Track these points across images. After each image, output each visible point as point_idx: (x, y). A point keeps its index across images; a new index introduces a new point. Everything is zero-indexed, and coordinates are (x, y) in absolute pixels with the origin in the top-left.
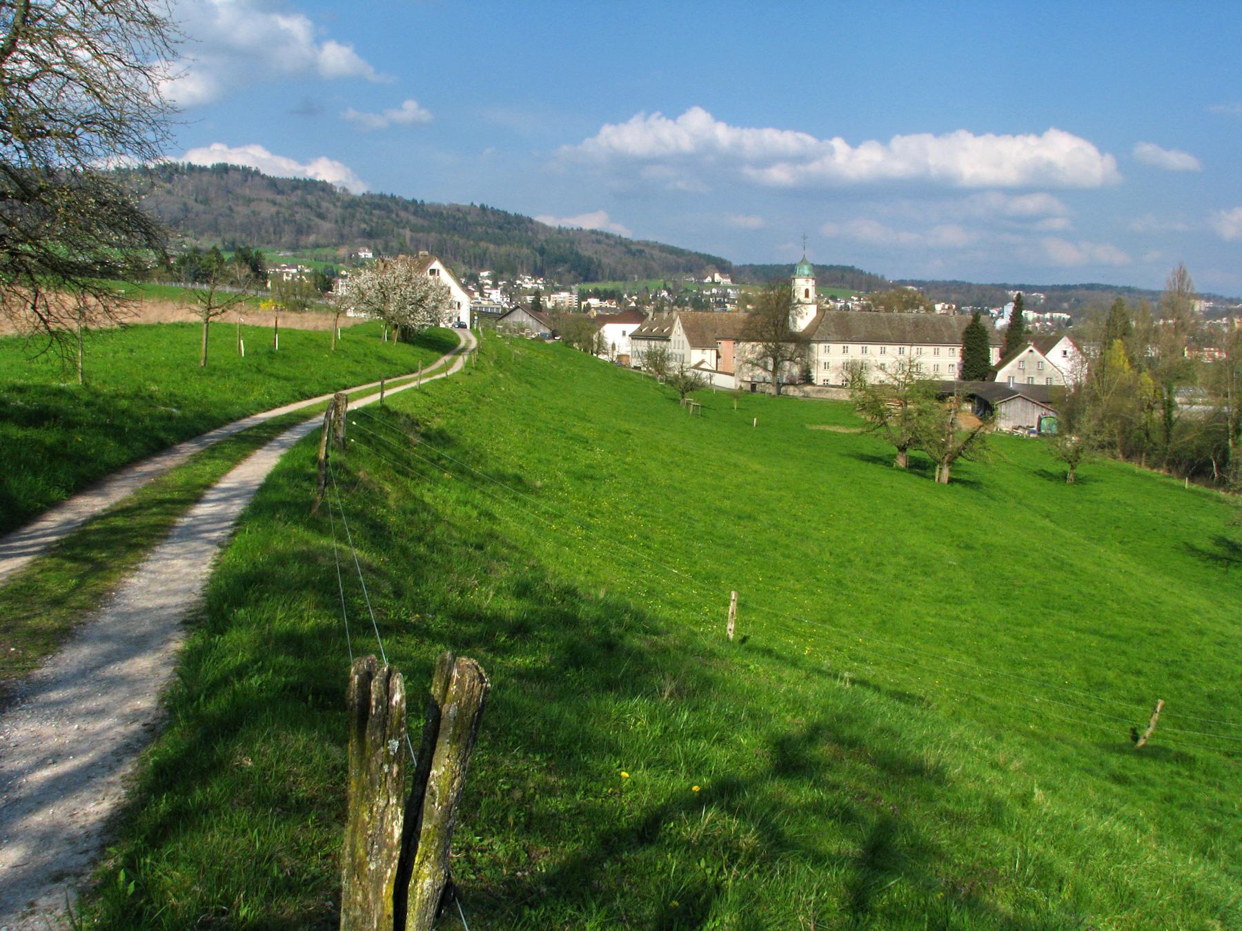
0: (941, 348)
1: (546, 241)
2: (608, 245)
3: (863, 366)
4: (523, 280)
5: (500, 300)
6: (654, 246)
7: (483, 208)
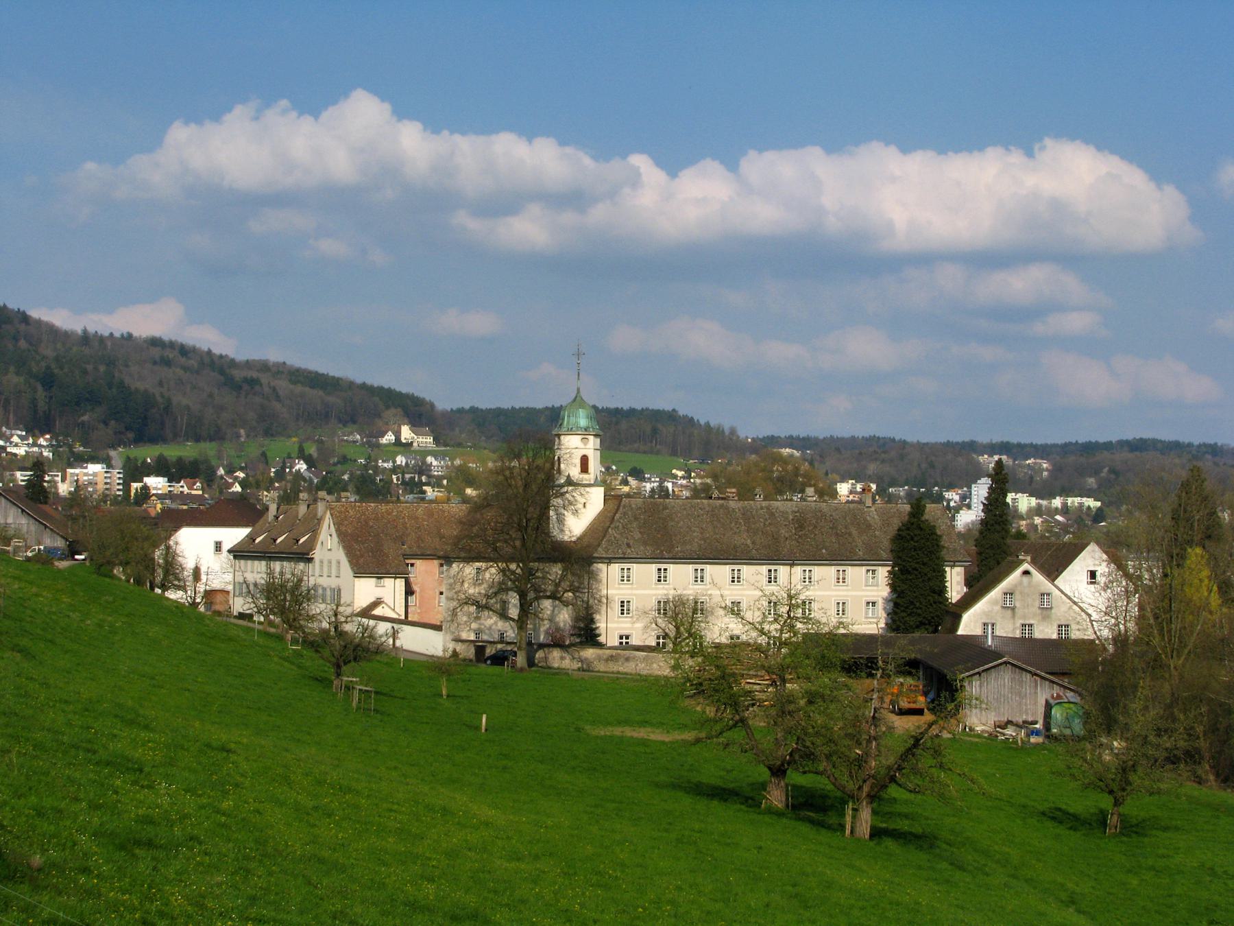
0: (849, 569)
1: (57, 359)
2: (185, 369)
6: (280, 370)
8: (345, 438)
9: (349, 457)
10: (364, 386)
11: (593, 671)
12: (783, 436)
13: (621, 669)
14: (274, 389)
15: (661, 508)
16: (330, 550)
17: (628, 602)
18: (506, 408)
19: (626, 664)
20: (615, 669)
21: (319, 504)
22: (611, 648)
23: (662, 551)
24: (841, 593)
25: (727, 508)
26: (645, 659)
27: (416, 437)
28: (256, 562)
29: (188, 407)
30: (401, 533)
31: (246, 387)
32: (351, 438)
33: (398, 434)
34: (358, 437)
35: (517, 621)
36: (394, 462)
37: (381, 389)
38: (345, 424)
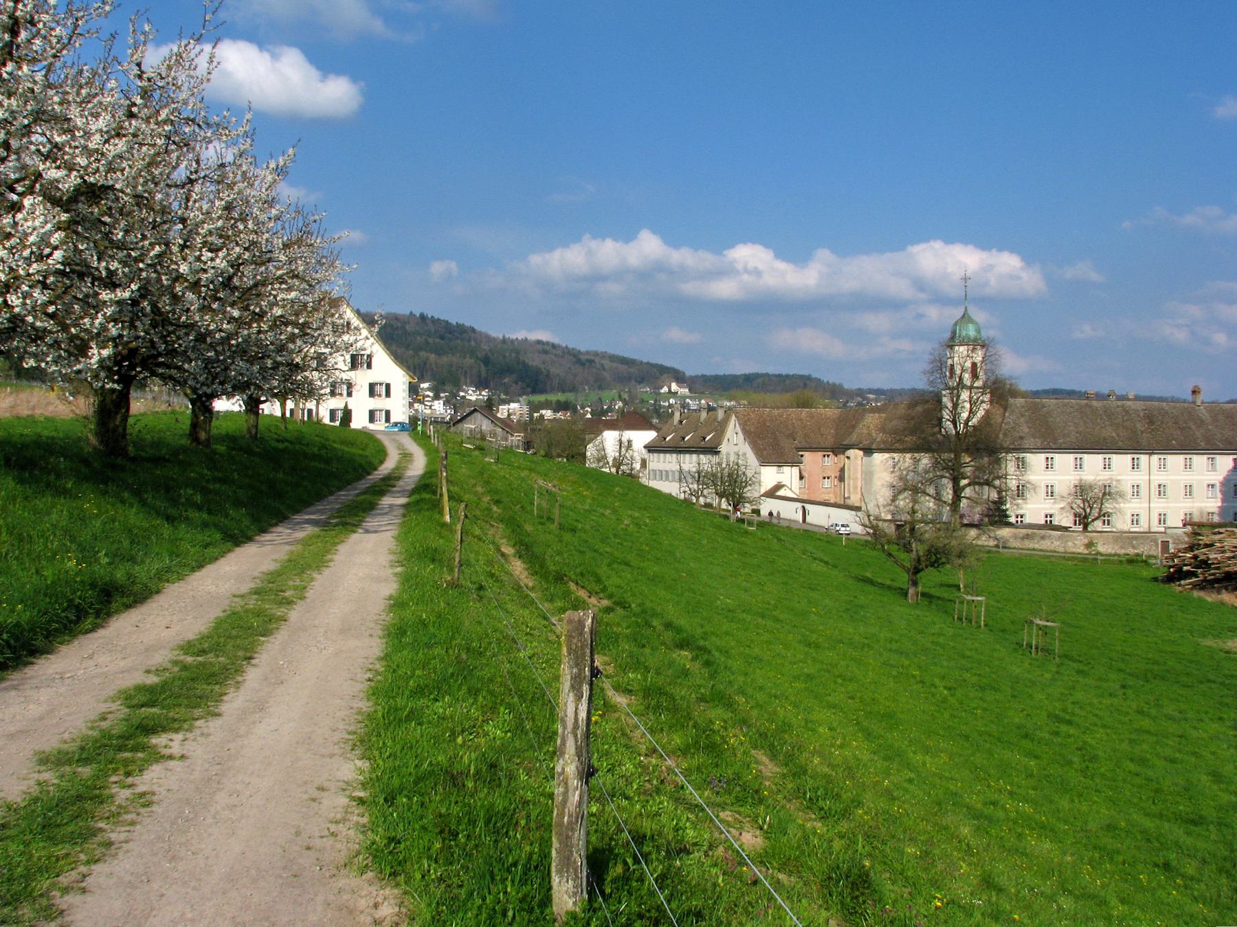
0: (1195, 457)
1: (490, 350)
2: (556, 355)
3: (1107, 492)
4: (466, 392)
5: (443, 411)
6: (604, 355)
7: (423, 317)
10: (648, 363)
13: (1037, 546)
14: (602, 365)
19: (1042, 542)
20: (1031, 546)
22: (1031, 526)
24: (1188, 478)
25: (1091, 407)
26: (1060, 537)
28: (668, 455)
29: (558, 375)
31: (587, 364)
38: (640, 383)
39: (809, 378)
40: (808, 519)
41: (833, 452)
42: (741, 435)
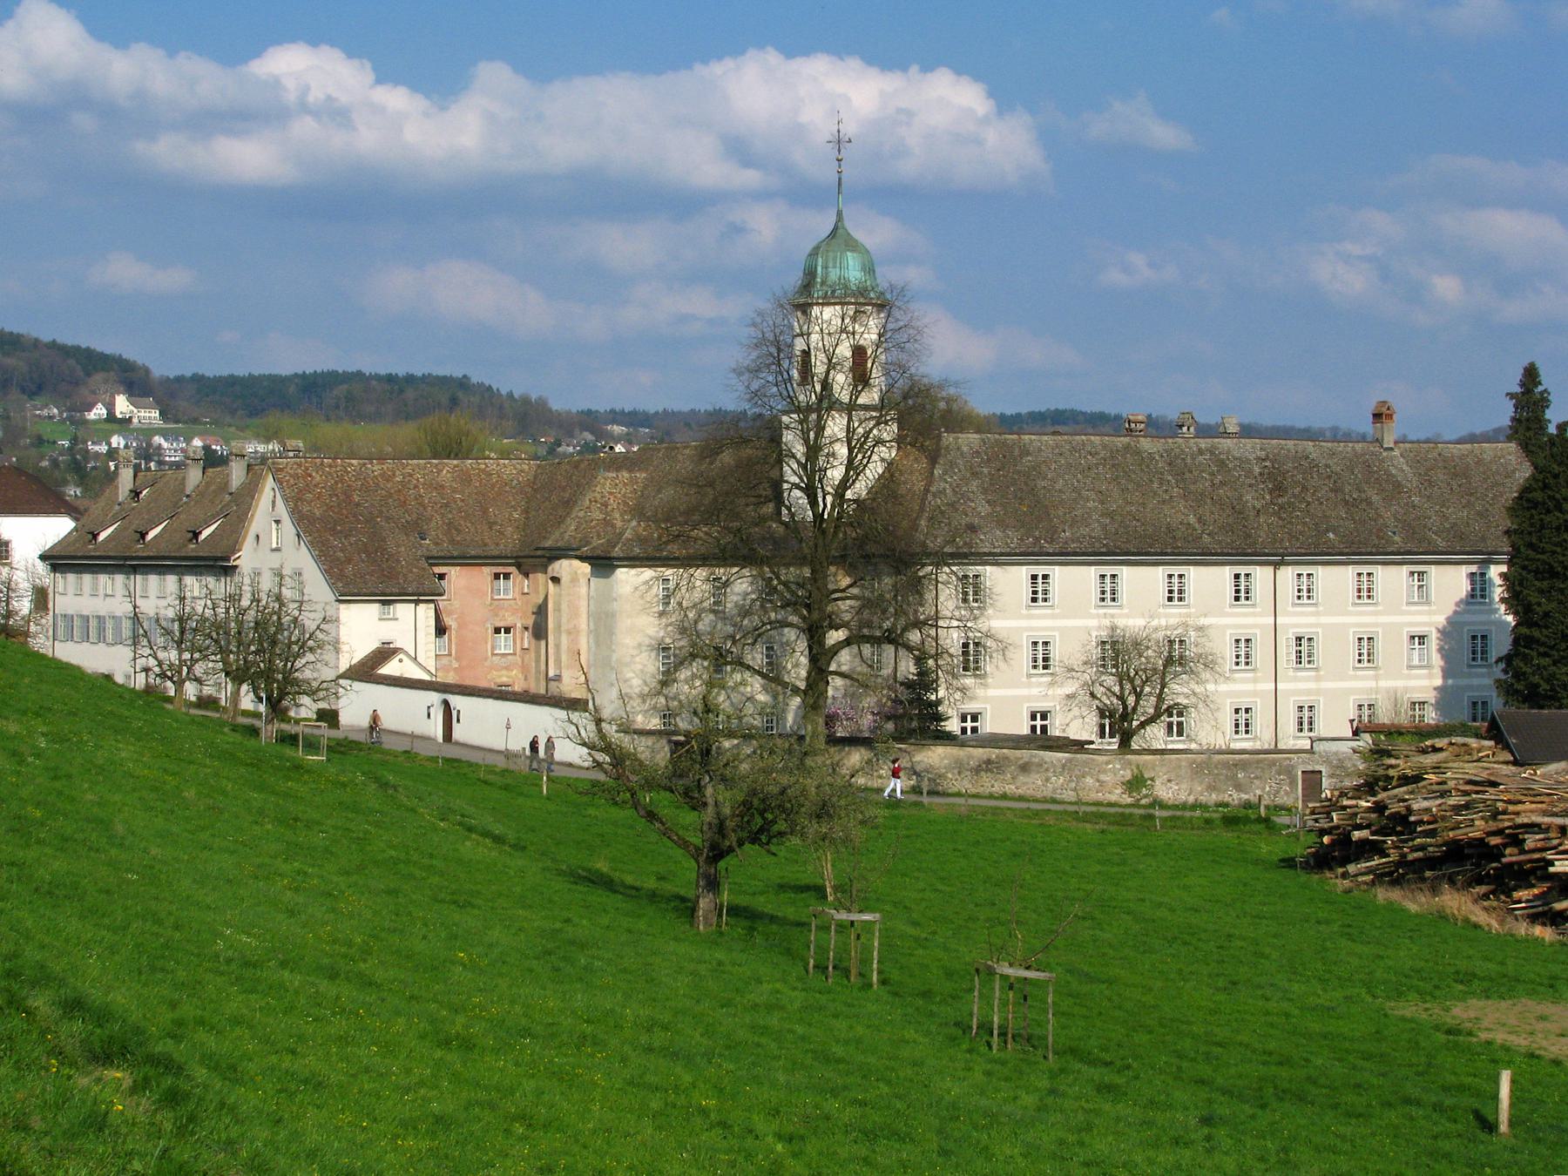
0: (1321, 572)
8: (38, 412)
9: (45, 438)
10: (53, 345)
11: (945, 794)
12: (602, 411)
13: (1010, 789)
15: (1016, 452)
16: (277, 550)
17: (1046, 643)
18: (241, 375)
19: (1022, 778)
20: (997, 788)
21: (233, 464)
22: (996, 741)
23: (1037, 539)
25: (1138, 452)
27: (135, 411)
30: (415, 515)
32: (45, 412)
33: (110, 407)
34: (55, 411)
35: (805, 692)
36: (109, 444)
37: (78, 348)
38: (32, 394)
39: (463, 383)
40: (459, 733)
41: (519, 566)
42: (288, 527)
